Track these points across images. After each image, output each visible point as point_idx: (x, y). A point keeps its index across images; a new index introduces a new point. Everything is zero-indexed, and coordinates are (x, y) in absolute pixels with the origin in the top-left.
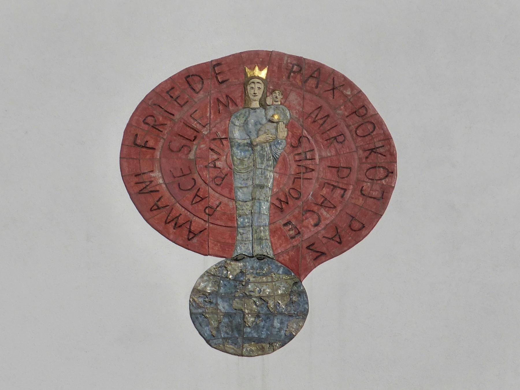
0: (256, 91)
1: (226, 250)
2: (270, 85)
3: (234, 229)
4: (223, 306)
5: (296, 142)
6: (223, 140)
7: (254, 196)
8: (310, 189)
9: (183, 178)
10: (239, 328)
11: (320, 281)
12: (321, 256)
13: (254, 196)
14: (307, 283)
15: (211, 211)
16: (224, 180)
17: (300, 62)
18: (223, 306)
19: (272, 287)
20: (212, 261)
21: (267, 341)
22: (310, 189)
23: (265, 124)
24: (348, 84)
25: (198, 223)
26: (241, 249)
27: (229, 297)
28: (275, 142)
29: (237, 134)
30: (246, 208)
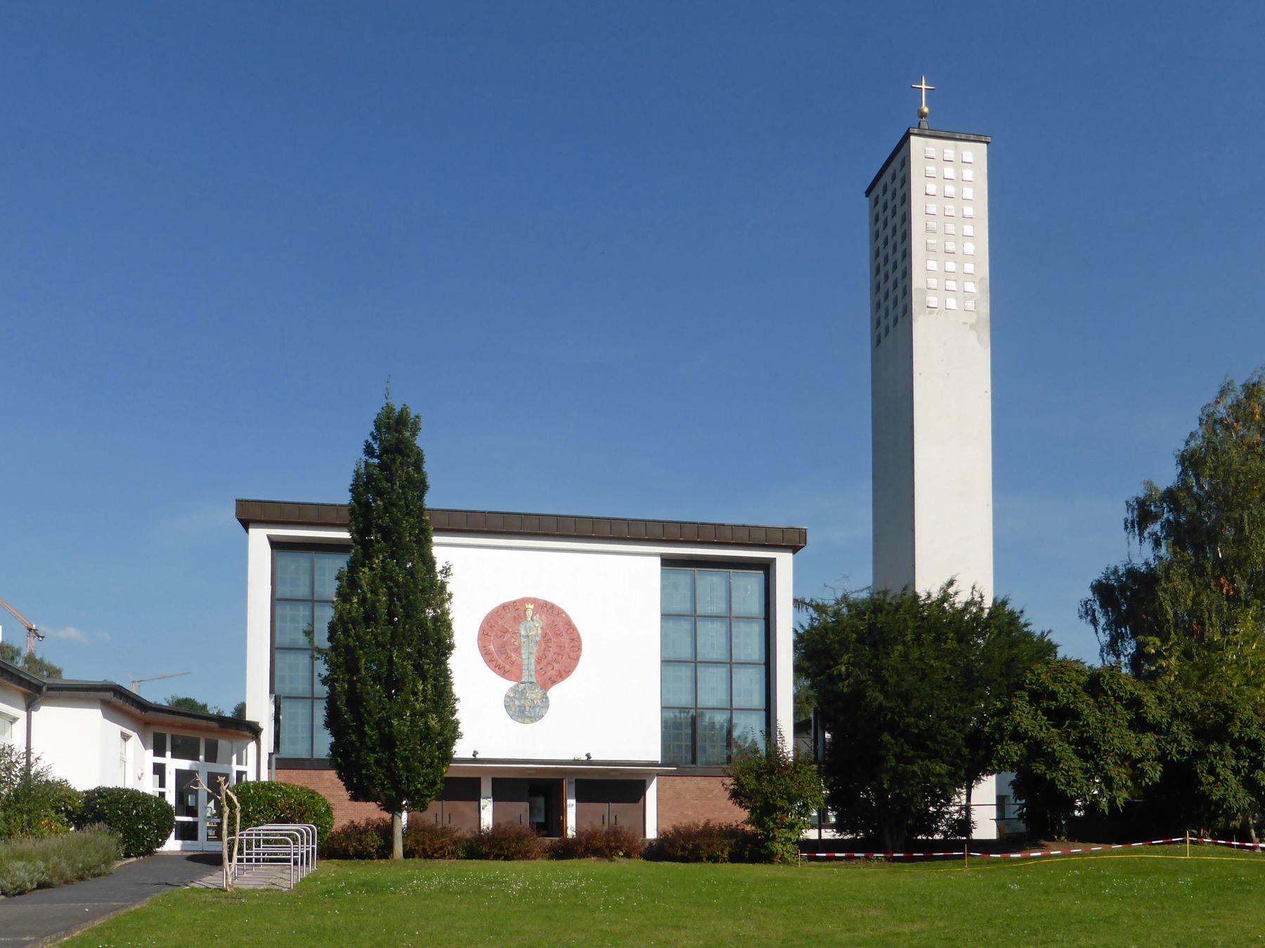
0: (529, 613)
1: (518, 678)
2: (535, 611)
3: (521, 670)
4: (517, 703)
5: (545, 635)
6: (516, 634)
7: (528, 657)
8: (550, 656)
9: (502, 649)
10: (523, 712)
11: (554, 692)
12: (554, 683)
13: (528, 657)
14: (549, 693)
15: (512, 663)
16: (517, 650)
17: (546, 603)
18: (517, 703)
19: (535, 694)
20: (513, 684)
21: (535, 718)
22: (550, 656)
23: (533, 627)
24: (563, 612)
25: (508, 667)
26: (524, 679)
27: (519, 699)
28: (536, 635)
29: (523, 632)
30: (526, 662)
